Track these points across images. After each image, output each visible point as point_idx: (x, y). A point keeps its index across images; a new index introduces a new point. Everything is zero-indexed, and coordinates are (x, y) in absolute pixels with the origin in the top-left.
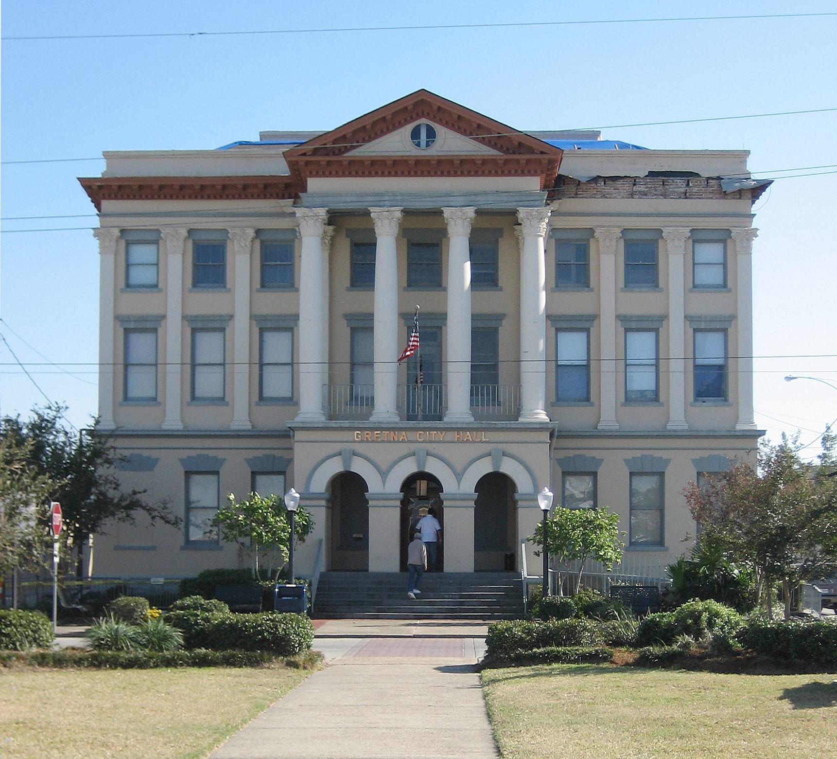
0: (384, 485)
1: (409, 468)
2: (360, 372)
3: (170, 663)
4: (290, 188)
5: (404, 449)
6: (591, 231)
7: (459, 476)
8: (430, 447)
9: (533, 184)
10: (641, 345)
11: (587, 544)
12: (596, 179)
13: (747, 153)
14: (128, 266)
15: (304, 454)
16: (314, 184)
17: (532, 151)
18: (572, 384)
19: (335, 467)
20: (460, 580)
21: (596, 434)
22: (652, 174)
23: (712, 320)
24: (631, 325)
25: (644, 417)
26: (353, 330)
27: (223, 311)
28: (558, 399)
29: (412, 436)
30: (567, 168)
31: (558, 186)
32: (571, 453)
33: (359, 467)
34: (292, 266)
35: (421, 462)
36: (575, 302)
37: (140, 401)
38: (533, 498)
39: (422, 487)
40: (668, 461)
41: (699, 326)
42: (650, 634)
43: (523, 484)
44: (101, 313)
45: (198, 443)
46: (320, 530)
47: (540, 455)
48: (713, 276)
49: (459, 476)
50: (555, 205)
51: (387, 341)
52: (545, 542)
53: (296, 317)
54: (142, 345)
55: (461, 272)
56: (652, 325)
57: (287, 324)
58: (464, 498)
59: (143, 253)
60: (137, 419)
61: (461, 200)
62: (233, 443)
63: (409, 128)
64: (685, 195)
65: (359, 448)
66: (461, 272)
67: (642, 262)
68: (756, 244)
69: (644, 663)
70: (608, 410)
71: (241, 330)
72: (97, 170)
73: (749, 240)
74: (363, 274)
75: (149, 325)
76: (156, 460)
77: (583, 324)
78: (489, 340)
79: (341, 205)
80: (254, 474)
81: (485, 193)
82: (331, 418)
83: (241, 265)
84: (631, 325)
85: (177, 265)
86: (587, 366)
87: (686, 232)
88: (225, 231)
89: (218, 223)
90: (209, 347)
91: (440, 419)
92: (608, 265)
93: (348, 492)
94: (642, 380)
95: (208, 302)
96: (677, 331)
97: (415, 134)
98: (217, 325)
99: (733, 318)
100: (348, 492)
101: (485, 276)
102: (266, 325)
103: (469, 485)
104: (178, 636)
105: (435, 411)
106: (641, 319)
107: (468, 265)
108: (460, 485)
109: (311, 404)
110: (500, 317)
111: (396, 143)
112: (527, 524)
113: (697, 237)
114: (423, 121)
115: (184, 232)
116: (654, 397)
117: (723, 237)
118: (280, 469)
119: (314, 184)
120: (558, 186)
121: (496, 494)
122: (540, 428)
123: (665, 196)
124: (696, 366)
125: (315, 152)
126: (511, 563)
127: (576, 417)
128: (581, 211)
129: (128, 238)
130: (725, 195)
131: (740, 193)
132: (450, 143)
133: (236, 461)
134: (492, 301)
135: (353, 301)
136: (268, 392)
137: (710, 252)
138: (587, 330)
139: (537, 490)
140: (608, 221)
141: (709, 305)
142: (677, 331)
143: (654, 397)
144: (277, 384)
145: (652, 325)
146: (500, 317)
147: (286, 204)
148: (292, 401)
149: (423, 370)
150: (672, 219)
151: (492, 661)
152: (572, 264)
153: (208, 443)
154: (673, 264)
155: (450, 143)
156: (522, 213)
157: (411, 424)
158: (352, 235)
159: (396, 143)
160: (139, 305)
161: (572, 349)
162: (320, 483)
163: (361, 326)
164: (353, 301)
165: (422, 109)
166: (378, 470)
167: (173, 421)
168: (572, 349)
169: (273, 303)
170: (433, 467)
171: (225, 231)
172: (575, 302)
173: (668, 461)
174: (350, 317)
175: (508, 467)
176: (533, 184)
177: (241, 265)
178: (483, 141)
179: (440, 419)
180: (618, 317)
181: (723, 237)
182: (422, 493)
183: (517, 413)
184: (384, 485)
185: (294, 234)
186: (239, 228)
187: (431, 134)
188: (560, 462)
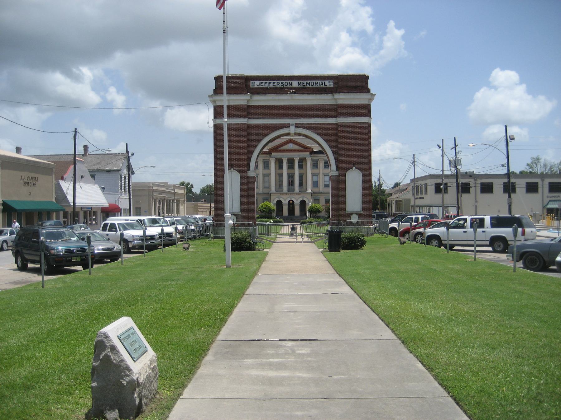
0: (285, 202)
7: (297, 201)
15: (272, 197)
19: (277, 199)
21: (319, 193)
33: (281, 199)
37: (267, 187)
43: (307, 202)
44: (363, 183)
47: (310, 197)
49: (297, 201)
57: (269, 175)
74: (281, 167)
93: (279, 203)
100: (279, 203)
101: (301, 167)
105: (293, 190)
108: (297, 202)
109: (273, 190)
118: (268, 200)
121: (303, 203)
122: (309, 193)
127: (316, 190)
134: (302, 171)
147: (268, 155)
148: (269, 187)
149: (291, 183)
152: (315, 165)
158: (279, 162)
162: (275, 202)
163: (281, 175)
168: (315, 179)
169: (266, 172)
174: (279, 174)
175: (305, 199)
182: (291, 205)
183: (306, 190)
184: (285, 202)
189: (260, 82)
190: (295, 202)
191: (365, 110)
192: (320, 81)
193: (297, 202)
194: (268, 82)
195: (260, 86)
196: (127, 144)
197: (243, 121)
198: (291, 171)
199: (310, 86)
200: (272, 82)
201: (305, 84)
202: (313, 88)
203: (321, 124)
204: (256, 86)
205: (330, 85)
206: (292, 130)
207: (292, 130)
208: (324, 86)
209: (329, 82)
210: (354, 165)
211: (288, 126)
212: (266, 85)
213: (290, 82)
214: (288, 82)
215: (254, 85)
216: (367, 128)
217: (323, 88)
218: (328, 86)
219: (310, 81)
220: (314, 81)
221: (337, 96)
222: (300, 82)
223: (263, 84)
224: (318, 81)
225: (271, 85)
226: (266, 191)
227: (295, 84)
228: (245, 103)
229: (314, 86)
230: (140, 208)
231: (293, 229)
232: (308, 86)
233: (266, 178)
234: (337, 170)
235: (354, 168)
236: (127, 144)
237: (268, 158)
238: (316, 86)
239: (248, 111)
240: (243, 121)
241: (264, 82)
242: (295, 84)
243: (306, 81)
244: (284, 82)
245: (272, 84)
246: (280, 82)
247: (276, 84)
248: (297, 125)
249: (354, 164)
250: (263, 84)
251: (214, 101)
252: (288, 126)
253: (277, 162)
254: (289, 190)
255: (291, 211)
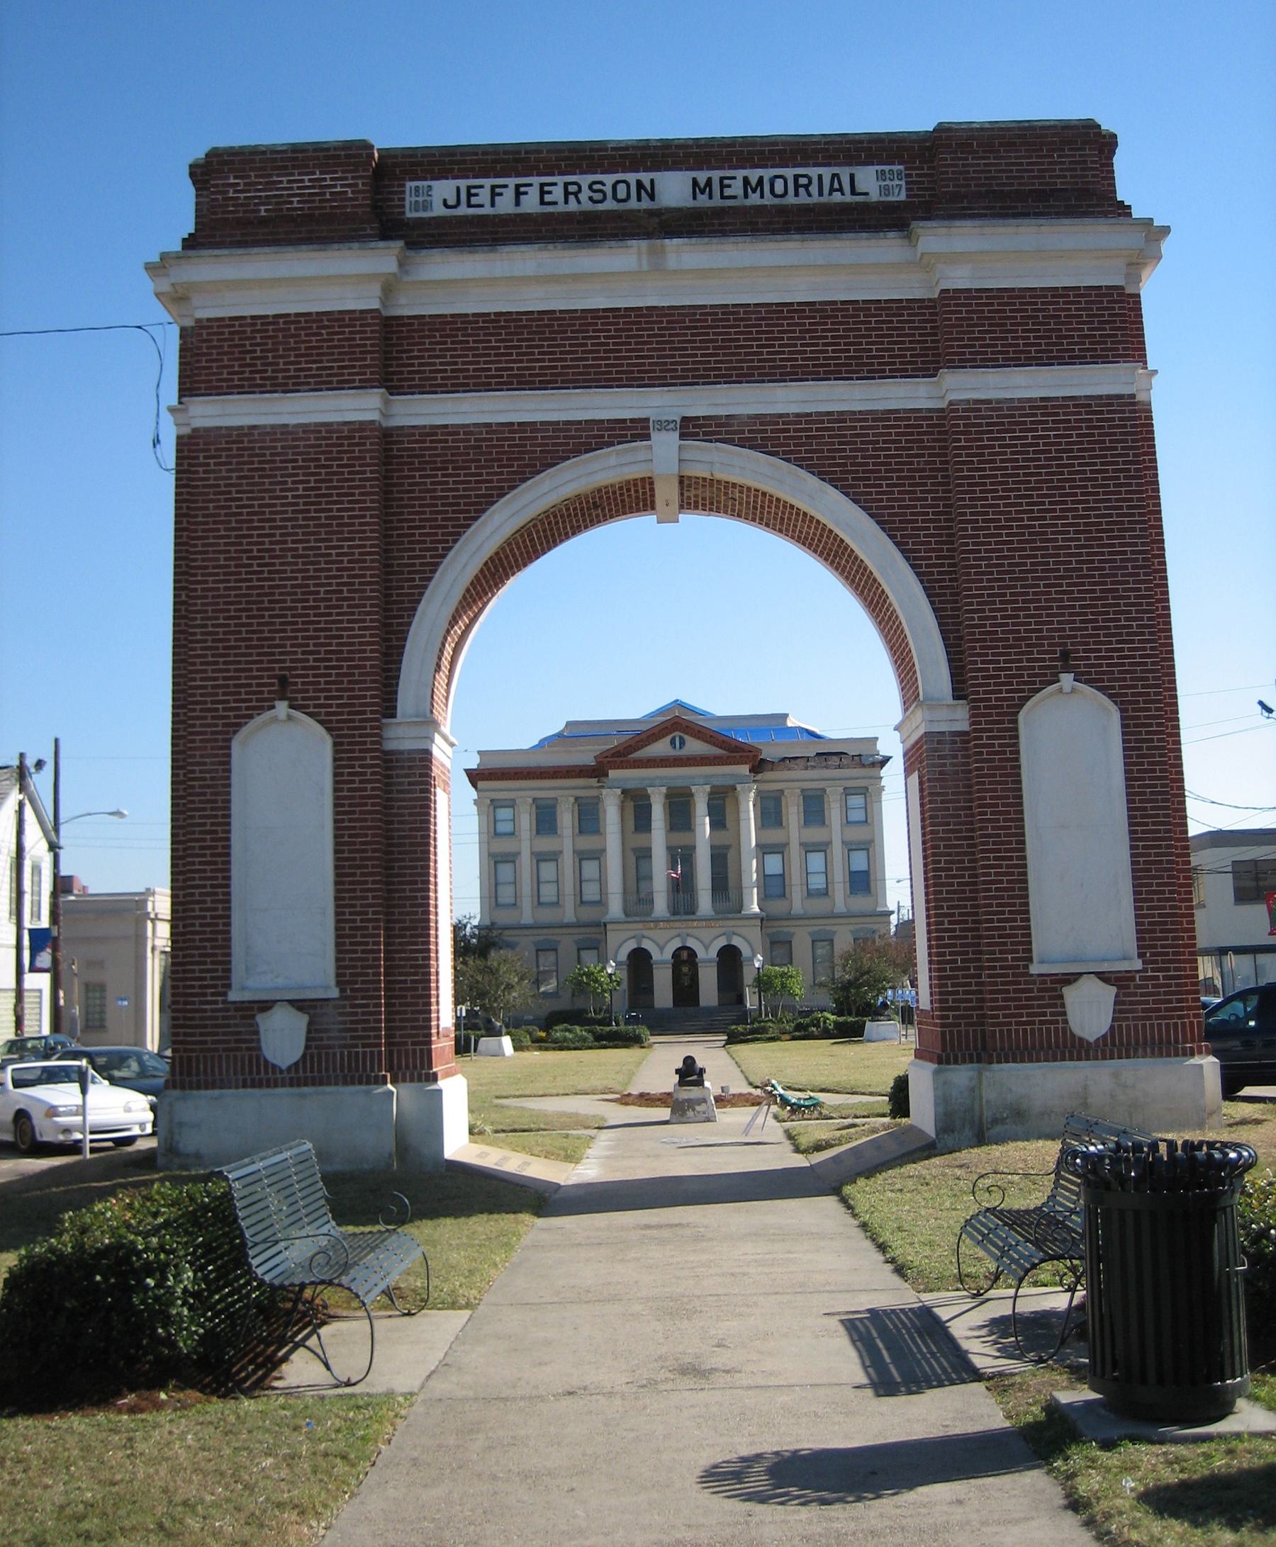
0: (662, 955)
1: (676, 944)
2: (643, 885)
3: (590, 1048)
4: (597, 771)
5: (674, 932)
6: (782, 791)
7: (707, 948)
8: (690, 931)
9: (744, 769)
10: (816, 861)
11: (783, 986)
12: (784, 759)
13: (877, 739)
14: (495, 821)
15: (613, 938)
16: (612, 773)
17: (744, 751)
18: (773, 887)
19: (632, 945)
20: (709, 1011)
21: (789, 917)
22: (818, 754)
23: (860, 843)
24: (809, 848)
25: (819, 906)
26: (638, 859)
27: (555, 848)
28: (766, 896)
29: (678, 924)
30: (768, 753)
31: (759, 766)
32: (774, 930)
33: (646, 944)
34: (598, 819)
35: (684, 941)
36: (774, 836)
38: (751, 960)
39: (685, 955)
40: (835, 933)
41: (851, 847)
42: (799, 1027)
45: (545, 931)
46: (625, 985)
47: (755, 933)
48: (857, 815)
49: (707, 948)
50: (759, 777)
51: (661, 872)
52: (759, 987)
53: (604, 850)
54: (505, 871)
55: (704, 826)
56: (822, 847)
57: (598, 855)
58: (710, 961)
59: (504, 813)
60: (504, 917)
61: (702, 781)
62: (564, 931)
63: (669, 738)
64: (839, 767)
65: (646, 933)
66: (704, 826)
67: (814, 808)
68: (884, 796)
69: (794, 1039)
70: (797, 902)
71: (568, 859)
72: (473, 763)
73: (880, 795)
75: (510, 858)
76: (517, 944)
77: (779, 849)
78: (722, 860)
79: (630, 785)
80: (579, 950)
81: (717, 776)
82: (626, 914)
83: (566, 819)
84: (809, 848)
85: (526, 821)
86: (783, 875)
87: (841, 789)
88: (556, 799)
89: (551, 794)
90: (548, 870)
91: (694, 913)
92: (793, 812)
93: (639, 961)
94: (817, 882)
95: (546, 844)
96: (837, 850)
97: (673, 742)
98: (554, 857)
99: (872, 841)
100: (639, 961)
101: (718, 823)
102: (582, 856)
103: (713, 953)
104: (590, 1037)
105: (691, 909)
106: (814, 844)
107: (707, 819)
108: (707, 953)
109: (615, 907)
110: (728, 847)
111: (661, 748)
112: (748, 977)
113: (848, 792)
114: (677, 733)
115: (530, 801)
116: (825, 893)
117: (864, 791)
119: (612, 773)
120: (759, 766)
121: (730, 959)
122: (754, 917)
123: (826, 767)
124: (850, 872)
125: (613, 755)
126: (740, 999)
127: (778, 907)
128: (774, 780)
129: (495, 804)
130: (864, 766)
131: (873, 765)
132: (695, 747)
133: (567, 943)
134: (724, 838)
135: (639, 841)
136: (585, 898)
137: (856, 801)
138: (782, 853)
139: (754, 956)
140: (792, 784)
141: (856, 834)
142: (837, 850)
143: (825, 893)
144: (591, 892)
145: (822, 847)
146: (728, 847)
147: (593, 782)
148: (601, 903)
149: (682, 888)
150: (831, 781)
151: (729, 1042)
152: (771, 813)
153: (551, 931)
154: (834, 814)
155: (695, 747)
156: (739, 787)
157: (677, 917)
159: (661, 748)
160: (505, 846)
161: (774, 864)
162: (623, 955)
163: (644, 854)
164: (638, 840)
165: (678, 722)
166: (657, 945)
167: (527, 918)
168: (774, 864)
169: (587, 842)
170: (691, 943)
171: (556, 799)
172: (774, 836)
173: (835, 933)
174: (635, 850)
175: (736, 941)
176: (744, 769)
177: (566, 819)
178: (714, 744)
179: (694, 913)
180: (801, 844)
181: (864, 791)
182: (685, 961)
183: (740, 907)
184: (662, 955)
185: (597, 800)
186: (565, 795)
187: (682, 743)
188: (768, 935)
189: (463, 184)
190: (701, 954)
191: (1109, 324)
192: (826, 172)
193: (707, 953)
194: (512, 182)
195: (463, 210)
196: (57, 741)
197: (358, 406)
198: (681, 838)
199: (768, 200)
200: (536, 180)
201: (736, 188)
202: (783, 210)
203: (841, 417)
204: (439, 211)
205: (886, 190)
206: (664, 455)
207: (664, 455)
208: (848, 198)
209: (881, 176)
210: (1066, 661)
211: (637, 430)
212: (503, 198)
213: (645, 177)
214: (632, 178)
215: (427, 206)
216: (1120, 447)
217: (845, 208)
218: (875, 196)
219: (768, 173)
220: (789, 173)
221: (936, 239)
222: (702, 177)
223: (484, 196)
224: (813, 172)
225: (531, 203)
226: (588, 914)
227: (674, 189)
228: (365, 299)
229: (791, 199)
230: (102, 988)
231: (690, 1073)
232: (754, 199)
233: (590, 868)
234: (958, 694)
235: (1067, 680)
236: (57, 741)
237: (594, 793)
238: (803, 199)
239: (392, 349)
240: (358, 406)
241: (488, 182)
242: (674, 189)
243: (740, 174)
244: (609, 179)
245: (534, 193)
246: (585, 180)
247: (557, 193)
248: (691, 428)
249: (1065, 656)
250: (484, 196)
251: (176, 299)
252: (637, 430)
253: (630, 805)
254: (674, 911)
255: (686, 990)
